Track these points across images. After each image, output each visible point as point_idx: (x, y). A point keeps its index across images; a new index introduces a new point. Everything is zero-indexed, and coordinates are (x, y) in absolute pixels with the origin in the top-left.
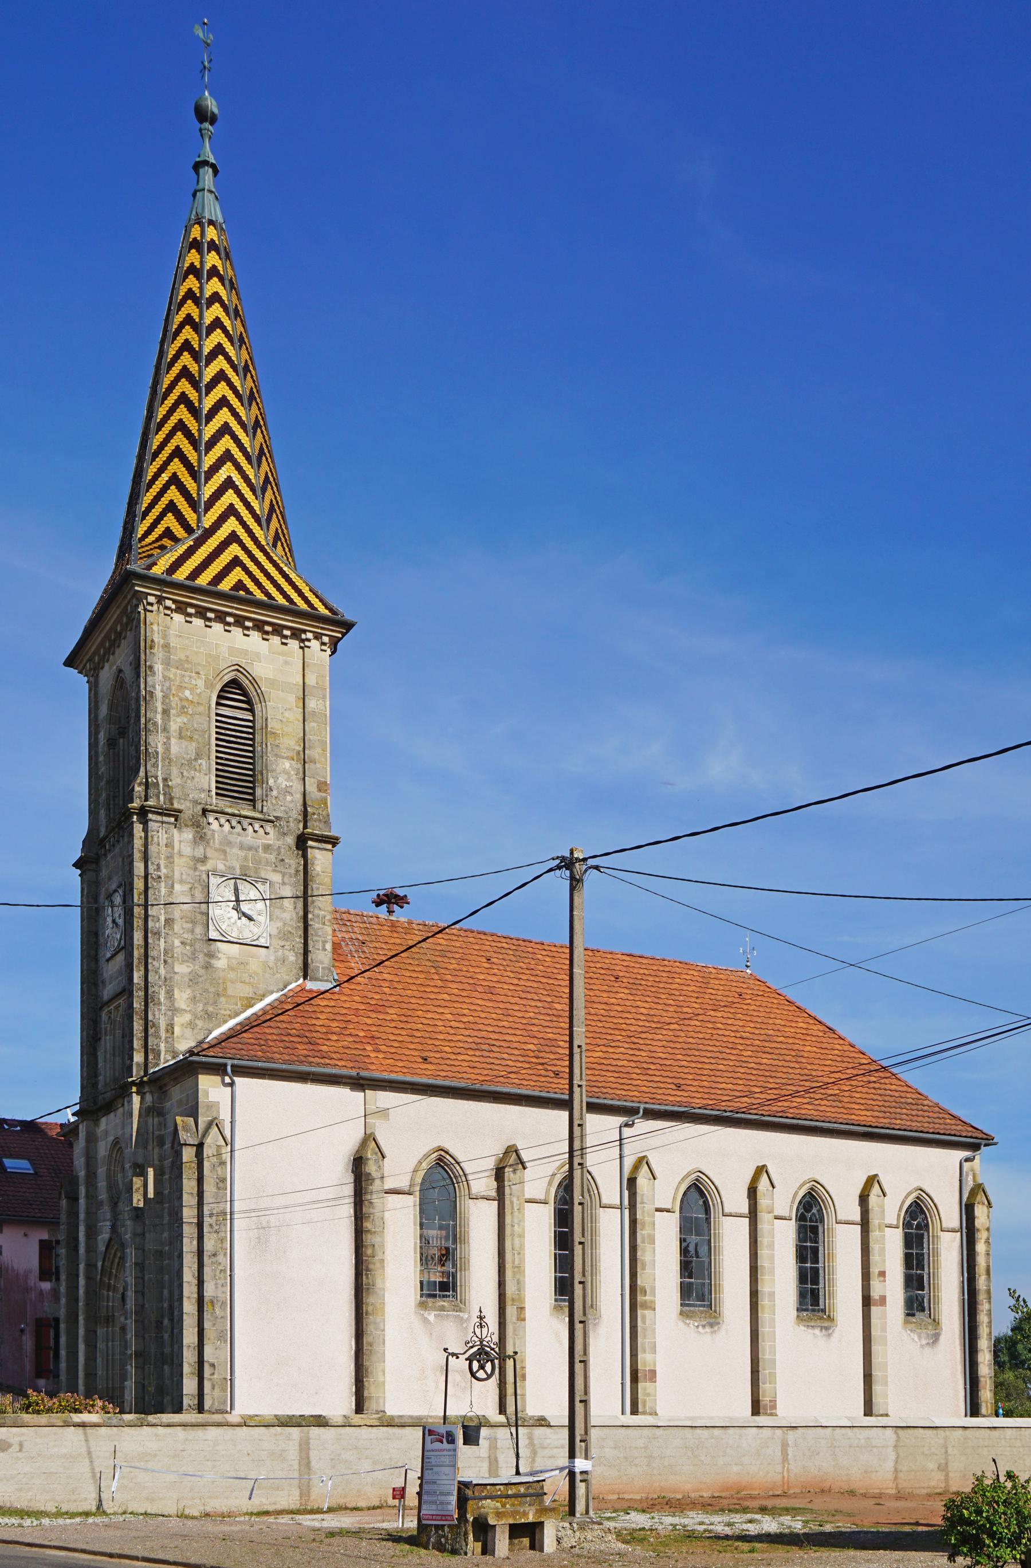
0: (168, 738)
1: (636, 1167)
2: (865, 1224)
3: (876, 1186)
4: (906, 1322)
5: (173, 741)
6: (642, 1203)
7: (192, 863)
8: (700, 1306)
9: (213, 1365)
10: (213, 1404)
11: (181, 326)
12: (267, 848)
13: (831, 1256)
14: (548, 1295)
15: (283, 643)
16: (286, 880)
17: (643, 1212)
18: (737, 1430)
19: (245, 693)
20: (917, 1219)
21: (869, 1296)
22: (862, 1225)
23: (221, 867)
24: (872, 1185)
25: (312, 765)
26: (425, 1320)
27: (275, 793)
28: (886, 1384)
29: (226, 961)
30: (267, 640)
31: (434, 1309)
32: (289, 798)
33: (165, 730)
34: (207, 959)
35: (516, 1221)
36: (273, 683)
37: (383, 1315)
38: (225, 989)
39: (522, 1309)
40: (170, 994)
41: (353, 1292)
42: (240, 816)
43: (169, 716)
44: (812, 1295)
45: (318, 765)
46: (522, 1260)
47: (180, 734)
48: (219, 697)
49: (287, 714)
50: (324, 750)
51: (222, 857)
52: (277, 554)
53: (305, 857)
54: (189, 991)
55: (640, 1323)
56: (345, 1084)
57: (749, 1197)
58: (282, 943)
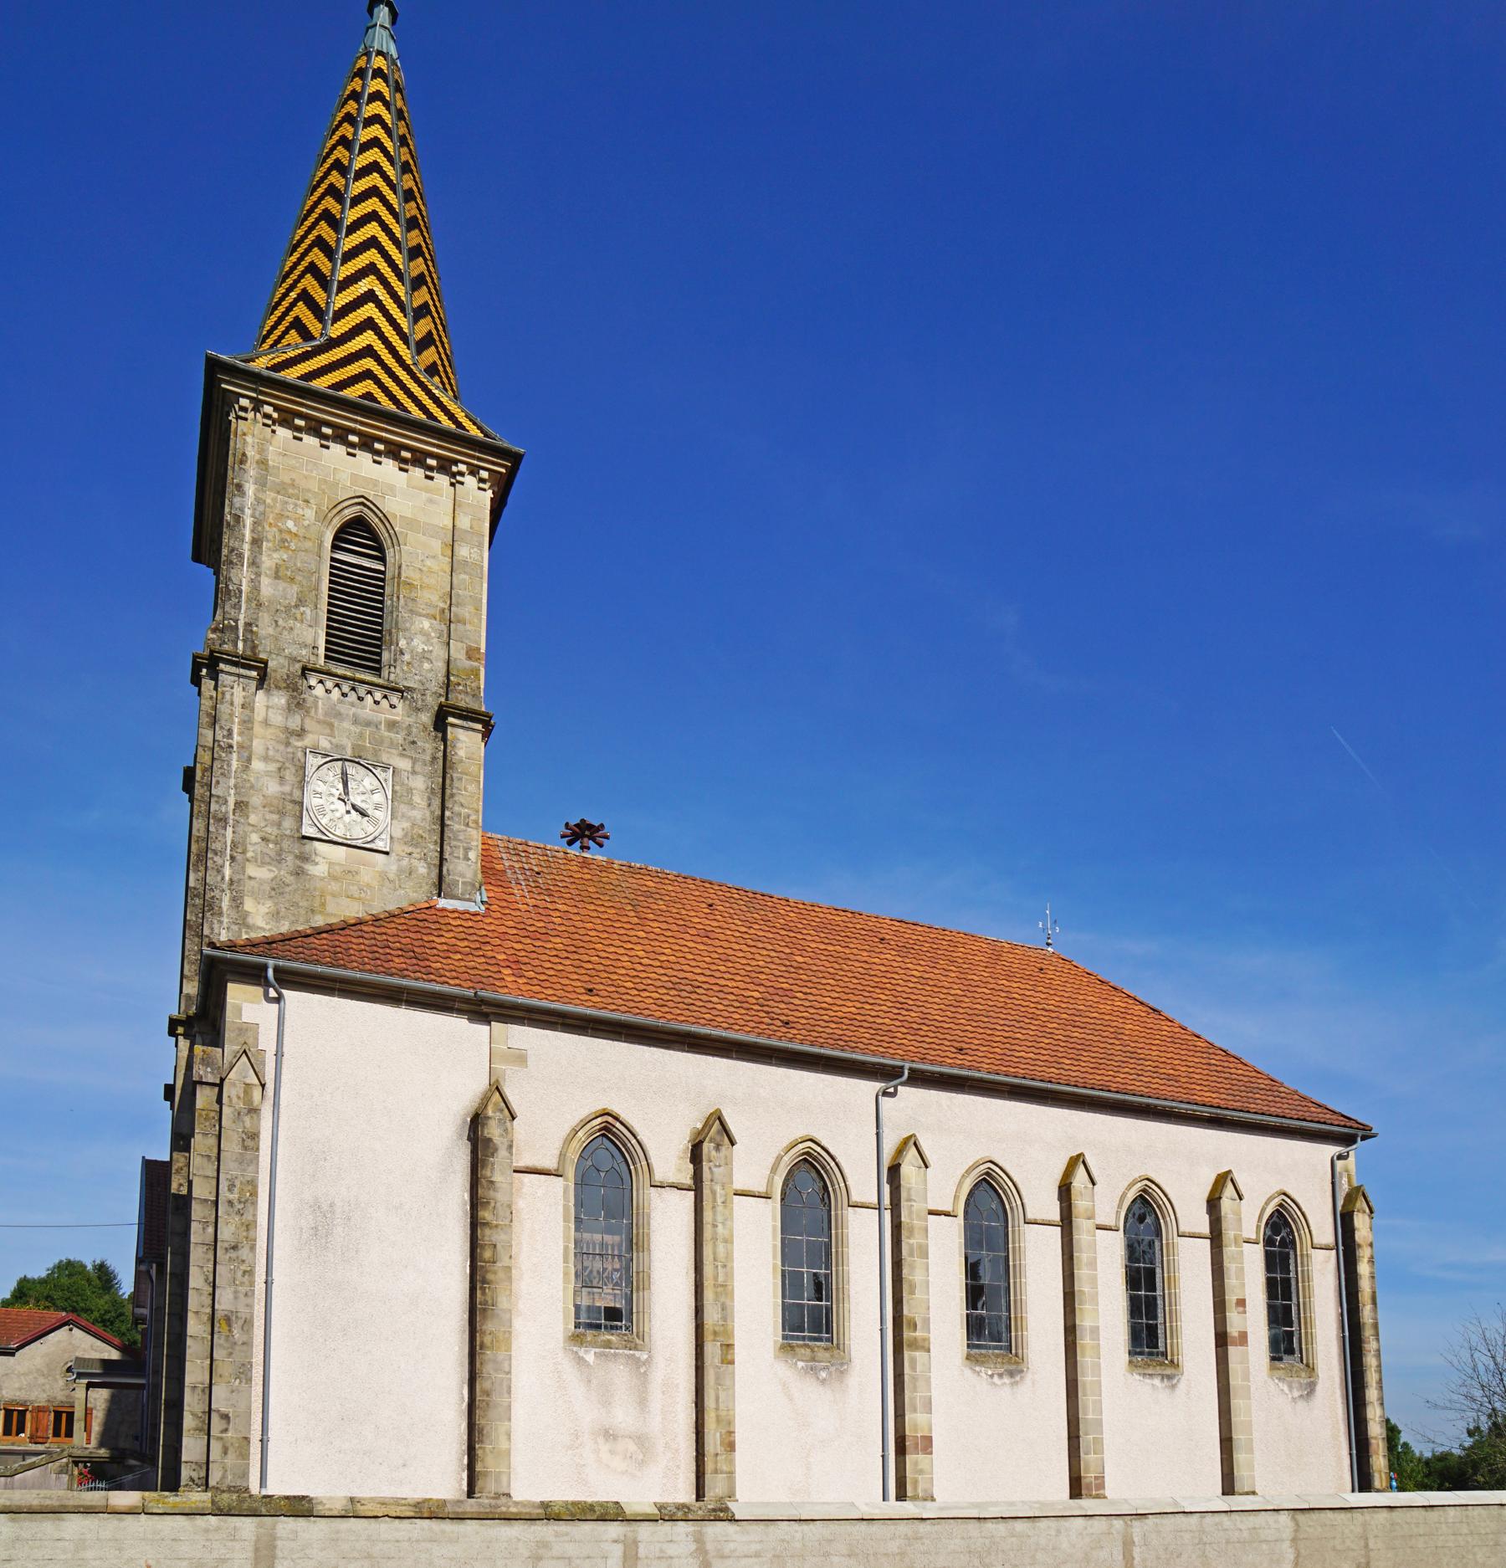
0: (258, 575)
1: (900, 1152)
2: (1216, 1237)
3: (1230, 1185)
4: (1272, 1368)
5: (265, 581)
6: (909, 1200)
7: (283, 736)
8: (996, 1348)
9: (226, 1417)
10: (224, 1477)
11: (334, 148)
12: (392, 725)
13: (1172, 1281)
14: (771, 1329)
15: (427, 477)
16: (418, 768)
17: (911, 1213)
18: (1052, 1523)
19: (374, 537)
20: (1281, 1234)
21: (1225, 1333)
22: (1212, 1240)
23: (324, 744)
24: (1223, 1185)
25: (460, 627)
26: (580, 1361)
27: (407, 657)
28: (1251, 1451)
29: (326, 867)
30: (406, 471)
31: (594, 1345)
32: (426, 666)
33: (254, 563)
34: (298, 862)
35: (720, 1218)
36: (412, 523)
37: (509, 1349)
38: (323, 905)
39: (728, 1347)
40: (237, 902)
41: (466, 1316)
42: (353, 680)
43: (260, 547)
44: (1148, 1336)
45: (468, 627)
46: (729, 1275)
47: (277, 572)
48: (336, 538)
49: (428, 563)
50: (478, 609)
51: (328, 731)
52: (434, 384)
53: (444, 740)
54: (269, 903)
55: (907, 1370)
56: (460, 1012)
57: (1060, 1198)
58: (410, 850)
